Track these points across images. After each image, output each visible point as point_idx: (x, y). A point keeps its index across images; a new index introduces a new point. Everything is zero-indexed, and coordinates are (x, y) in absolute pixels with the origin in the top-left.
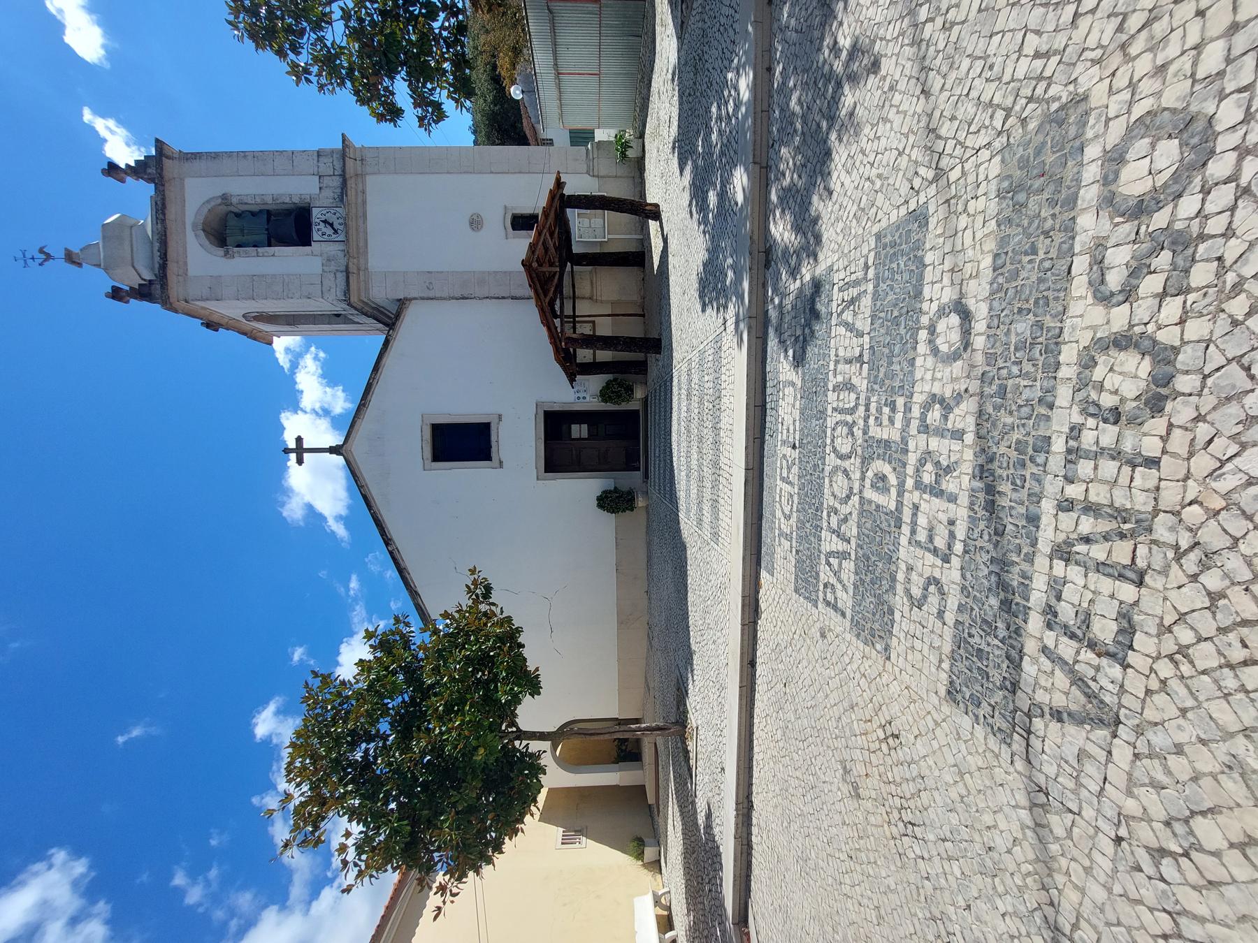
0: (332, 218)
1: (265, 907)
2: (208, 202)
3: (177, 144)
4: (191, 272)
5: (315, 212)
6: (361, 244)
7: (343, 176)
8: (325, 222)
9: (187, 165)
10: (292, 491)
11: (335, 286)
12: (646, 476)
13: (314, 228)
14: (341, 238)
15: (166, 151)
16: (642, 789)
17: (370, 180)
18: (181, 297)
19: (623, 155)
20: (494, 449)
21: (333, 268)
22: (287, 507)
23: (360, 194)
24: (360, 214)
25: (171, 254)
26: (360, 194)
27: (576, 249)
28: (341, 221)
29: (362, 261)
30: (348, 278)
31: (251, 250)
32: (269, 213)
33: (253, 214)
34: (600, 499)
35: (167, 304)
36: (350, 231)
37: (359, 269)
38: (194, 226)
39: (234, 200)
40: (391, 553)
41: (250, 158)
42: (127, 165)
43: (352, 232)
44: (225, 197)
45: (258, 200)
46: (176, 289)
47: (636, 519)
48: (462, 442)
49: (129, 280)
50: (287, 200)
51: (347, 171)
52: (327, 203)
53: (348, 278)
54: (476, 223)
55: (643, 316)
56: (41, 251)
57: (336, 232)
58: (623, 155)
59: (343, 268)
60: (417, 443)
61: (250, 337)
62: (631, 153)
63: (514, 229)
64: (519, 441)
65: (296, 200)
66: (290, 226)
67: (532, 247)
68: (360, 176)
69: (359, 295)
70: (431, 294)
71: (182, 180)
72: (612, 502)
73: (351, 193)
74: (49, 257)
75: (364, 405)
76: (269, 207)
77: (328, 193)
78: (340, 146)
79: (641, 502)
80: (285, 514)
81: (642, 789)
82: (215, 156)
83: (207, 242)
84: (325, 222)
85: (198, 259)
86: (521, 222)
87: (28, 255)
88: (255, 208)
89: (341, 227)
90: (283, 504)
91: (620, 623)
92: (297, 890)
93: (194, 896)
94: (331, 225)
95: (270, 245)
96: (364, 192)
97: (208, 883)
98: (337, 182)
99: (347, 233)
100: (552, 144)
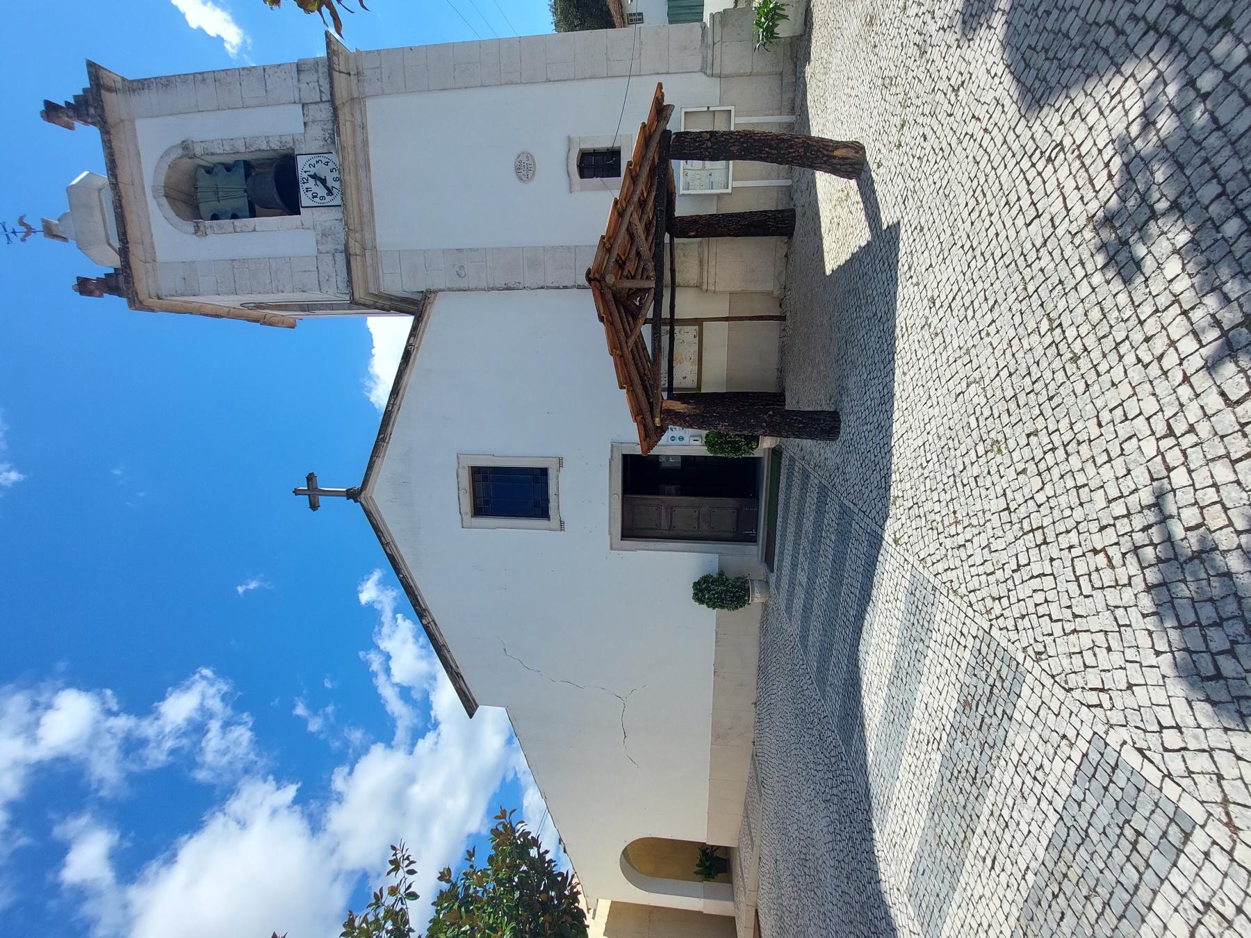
0: (322, 170)
1: (374, 742)
2: (166, 153)
3: (121, 66)
4: (161, 257)
5: (301, 162)
6: (365, 209)
7: (332, 101)
8: (314, 177)
9: (134, 99)
10: (378, 377)
11: (334, 270)
12: (768, 558)
13: (303, 187)
14: (338, 201)
15: (106, 81)
16: (731, 921)
17: (370, 104)
18: (153, 294)
19: (770, 33)
20: (552, 505)
21: (331, 247)
22: (374, 392)
23: (359, 130)
24: (361, 161)
25: (133, 233)
26: (359, 130)
27: (682, 209)
28: (336, 174)
29: (367, 236)
30: (348, 263)
31: (226, 223)
32: (247, 165)
33: (228, 168)
34: (697, 586)
35: (135, 302)
36: (346, 191)
37: (364, 248)
38: (155, 189)
39: (198, 150)
40: (426, 628)
41: (210, 81)
42: (67, 103)
43: (352, 192)
44: (185, 146)
45: (228, 148)
46: (144, 284)
47: (748, 617)
48: (510, 492)
49: (96, 272)
50: (264, 147)
51: (337, 95)
52: (316, 146)
53: (348, 263)
54: (525, 169)
55: (782, 318)
56: (22, 223)
57: (330, 192)
58: (770, 33)
59: (342, 248)
60: (453, 494)
61: (264, 323)
62: (784, 30)
63: (582, 176)
64: (588, 494)
65: (275, 145)
66: (271, 184)
67: (619, 211)
68: (357, 101)
69: (366, 288)
70: (463, 284)
71: (132, 121)
72: (718, 591)
73: (346, 129)
74: (30, 231)
75: (383, 440)
76: (247, 157)
77: (317, 131)
78: (322, 53)
79: (757, 598)
80: (372, 400)
81: (731, 921)
82: (166, 83)
83: (172, 214)
84: (314, 177)
85: (167, 239)
86: (597, 163)
87: (9, 230)
88: (229, 160)
89: (337, 185)
90: (370, 391)
91: (716, 737)
92: (401, 734)
93: (315, 725)
94: (323, 181)
95: (253, 214)
96: (363, 127)
97: (326, 717)
98: (324, 112)
99: (343, 194)
100: (641, 20)
